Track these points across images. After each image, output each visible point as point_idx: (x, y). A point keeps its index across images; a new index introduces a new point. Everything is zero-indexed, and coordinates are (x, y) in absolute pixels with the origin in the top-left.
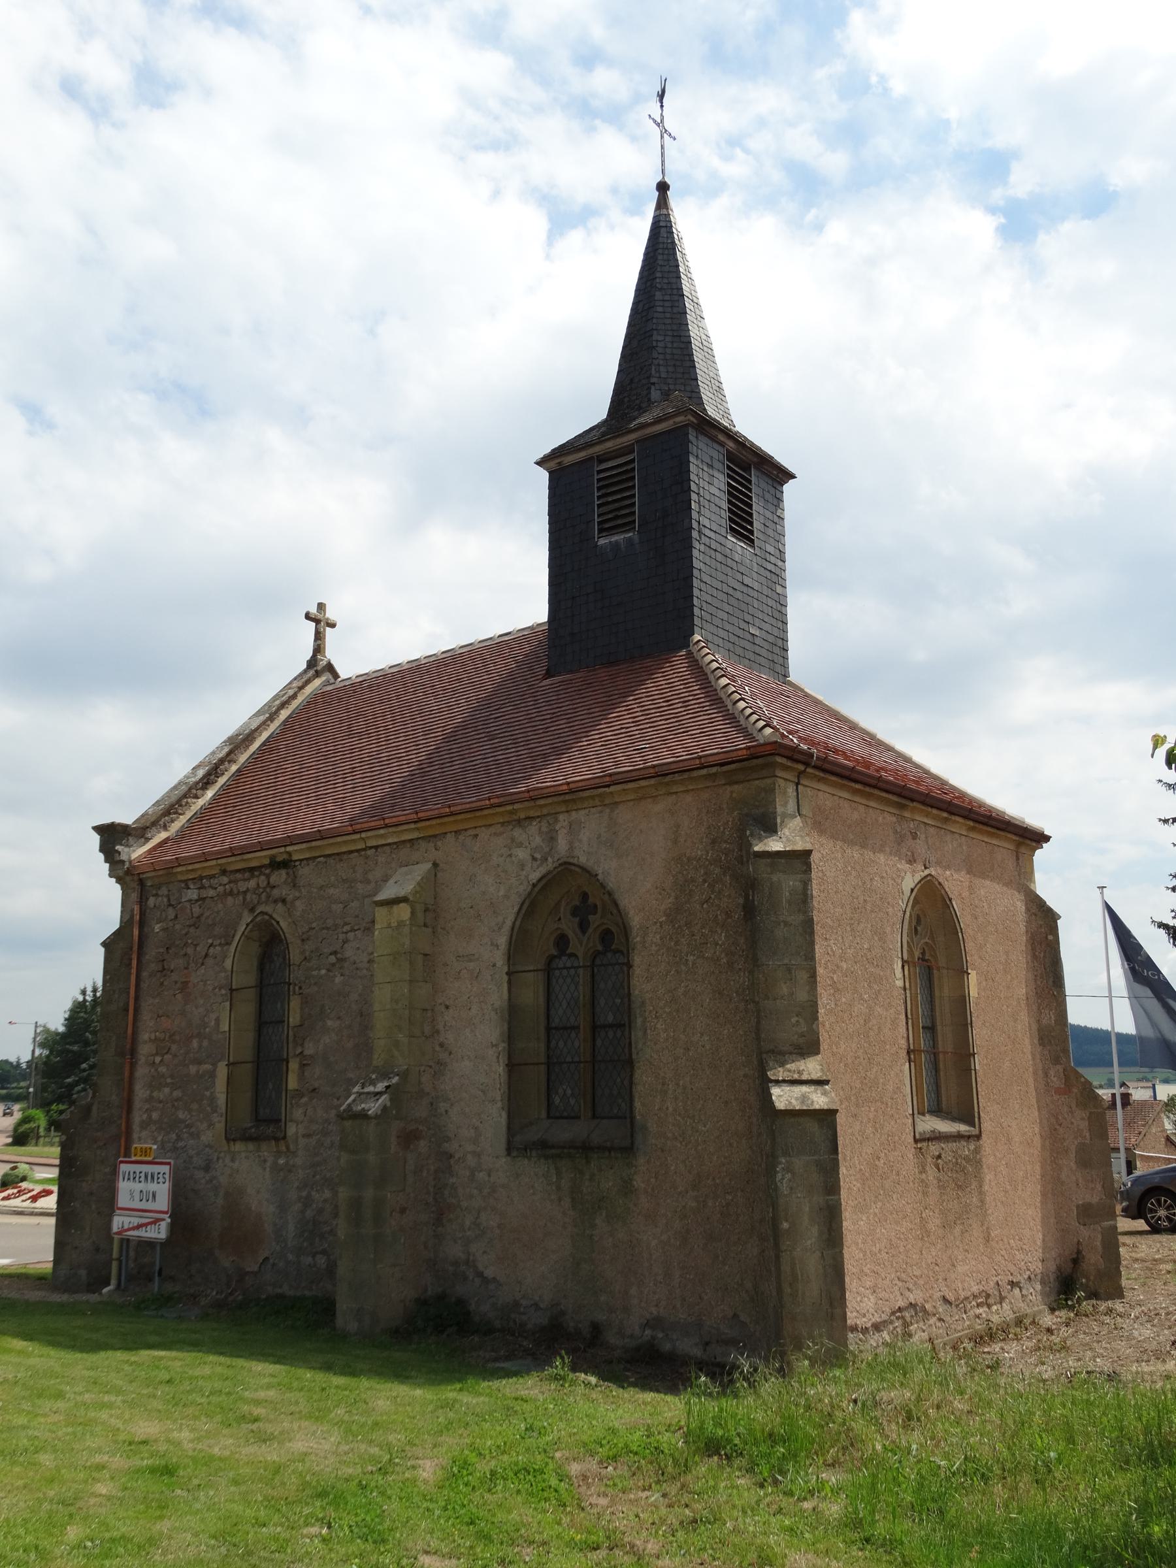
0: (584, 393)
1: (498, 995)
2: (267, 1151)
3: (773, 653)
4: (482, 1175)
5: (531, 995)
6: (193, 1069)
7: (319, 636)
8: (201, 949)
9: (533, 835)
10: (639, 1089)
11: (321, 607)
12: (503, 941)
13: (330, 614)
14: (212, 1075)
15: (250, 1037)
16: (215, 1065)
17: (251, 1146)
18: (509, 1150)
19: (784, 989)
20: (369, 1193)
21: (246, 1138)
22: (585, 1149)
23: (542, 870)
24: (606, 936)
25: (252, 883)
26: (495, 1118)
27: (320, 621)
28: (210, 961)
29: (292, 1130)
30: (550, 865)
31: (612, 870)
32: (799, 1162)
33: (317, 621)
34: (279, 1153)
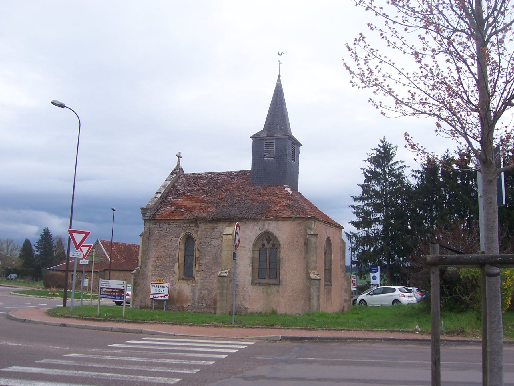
0: (258, 123)
1: (250, 255)
2: (190, 283)
3: (294, 186)
4: (245, 289)
5: (257, 255)
6: (168, 264)
7: (179, 160)
8: (170, 238)
9: (260, 225)
10: (281, 274)
11: (180, 153)
12: (252, 244)
13: (181, 155)
14: (174, 266)
15: (183, 259)
16: (174, 264)
17: (185, 281)
18: (252, 284)
19: (312, 258)
20: (225, 291)
21: (183, 279)
22: (269, 285)
23: (261, 232)
24: (273, 245)
25: (185, 225)
26: (249, 278)
27: (179, 157)
28: (172, 241)
29: (196, 279)
30: (263, 231)
31: (276, 233)
32: (314, 287)
33: (179, 157)
34: (193, 283)
